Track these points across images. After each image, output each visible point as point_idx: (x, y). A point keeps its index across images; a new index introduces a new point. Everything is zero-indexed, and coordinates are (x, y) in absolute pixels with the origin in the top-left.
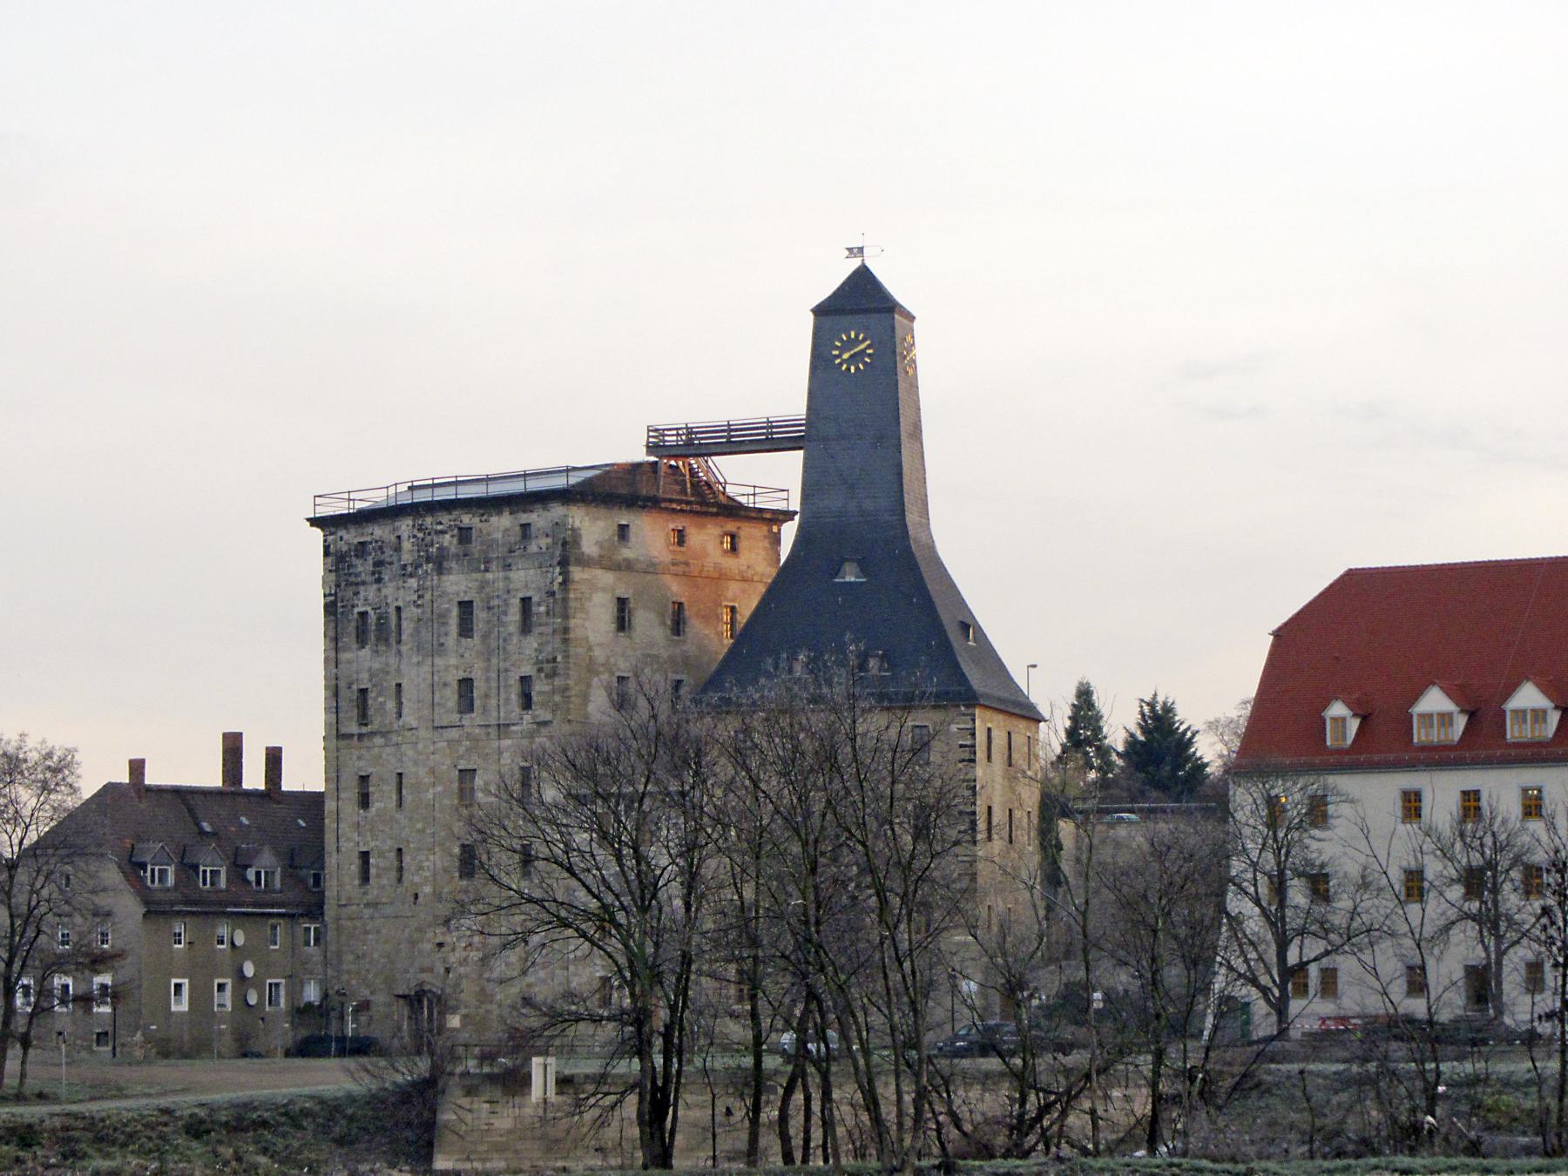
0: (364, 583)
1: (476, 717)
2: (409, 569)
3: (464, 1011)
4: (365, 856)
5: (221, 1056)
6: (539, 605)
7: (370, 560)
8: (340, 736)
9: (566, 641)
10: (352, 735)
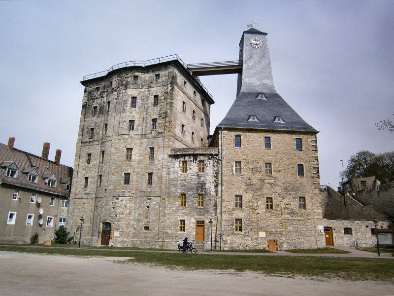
0: (97, 98)
1: (134, 132)
2: (115, 89)
3: (121, 230)
4: (87, 179)
5: (272, 82)
6: (161, 97)
7: (100, 92)
8: (82, 143)
9: (171, 106)
10: (87, 142)
